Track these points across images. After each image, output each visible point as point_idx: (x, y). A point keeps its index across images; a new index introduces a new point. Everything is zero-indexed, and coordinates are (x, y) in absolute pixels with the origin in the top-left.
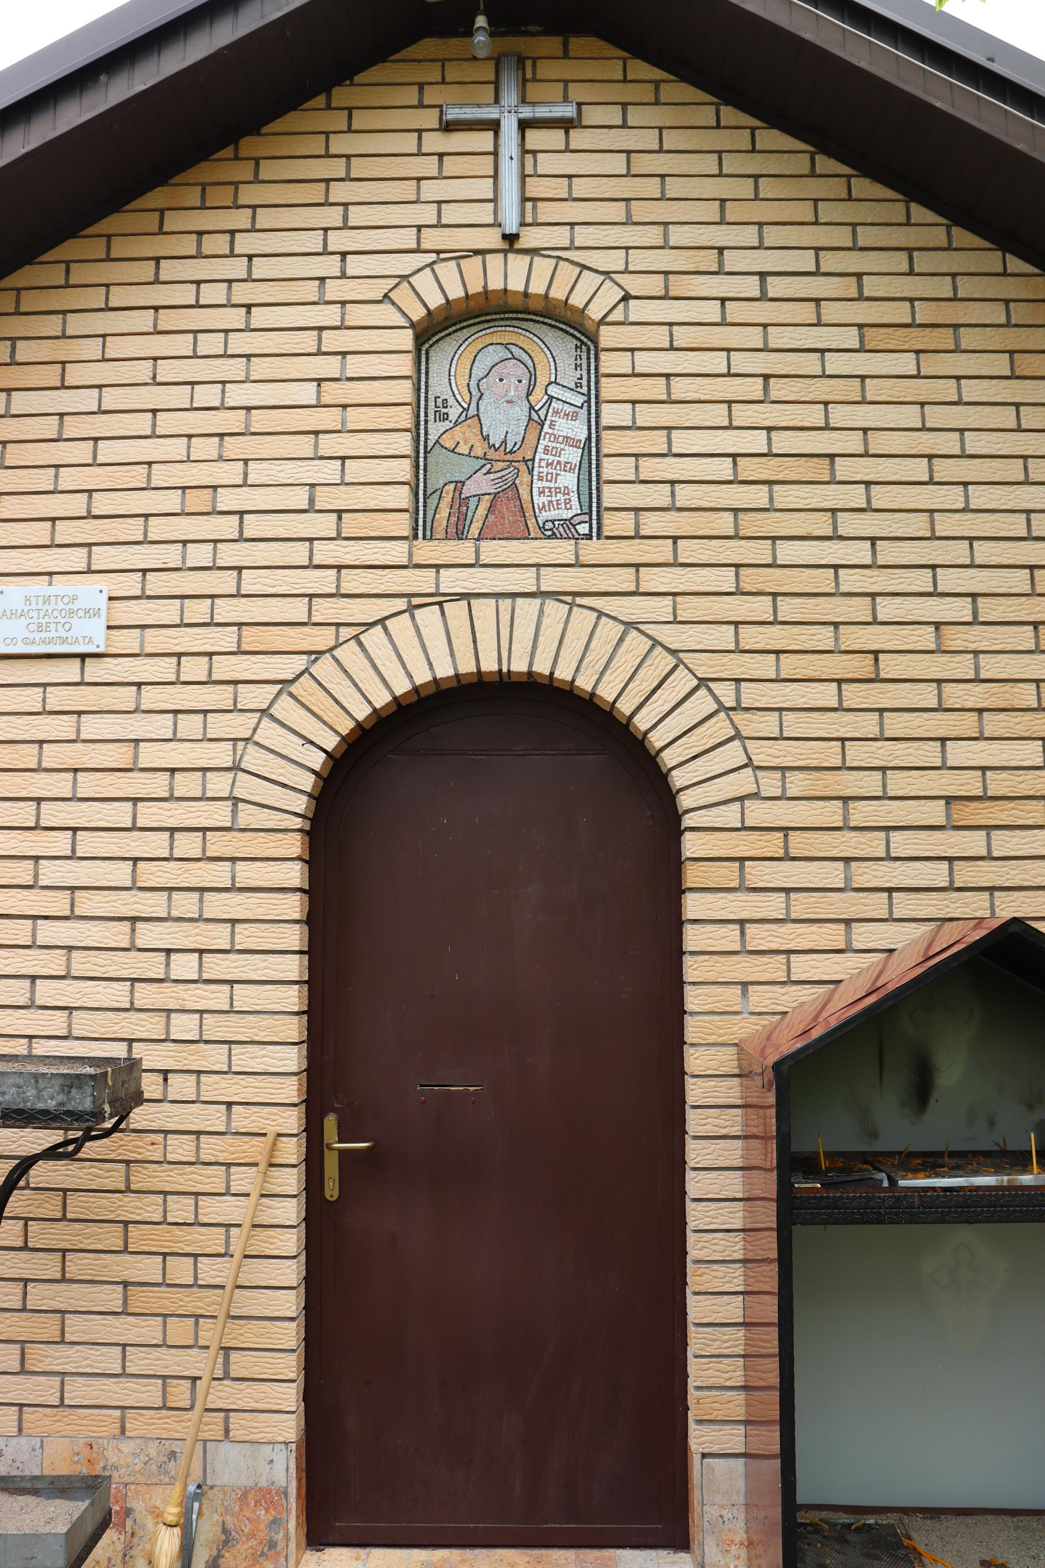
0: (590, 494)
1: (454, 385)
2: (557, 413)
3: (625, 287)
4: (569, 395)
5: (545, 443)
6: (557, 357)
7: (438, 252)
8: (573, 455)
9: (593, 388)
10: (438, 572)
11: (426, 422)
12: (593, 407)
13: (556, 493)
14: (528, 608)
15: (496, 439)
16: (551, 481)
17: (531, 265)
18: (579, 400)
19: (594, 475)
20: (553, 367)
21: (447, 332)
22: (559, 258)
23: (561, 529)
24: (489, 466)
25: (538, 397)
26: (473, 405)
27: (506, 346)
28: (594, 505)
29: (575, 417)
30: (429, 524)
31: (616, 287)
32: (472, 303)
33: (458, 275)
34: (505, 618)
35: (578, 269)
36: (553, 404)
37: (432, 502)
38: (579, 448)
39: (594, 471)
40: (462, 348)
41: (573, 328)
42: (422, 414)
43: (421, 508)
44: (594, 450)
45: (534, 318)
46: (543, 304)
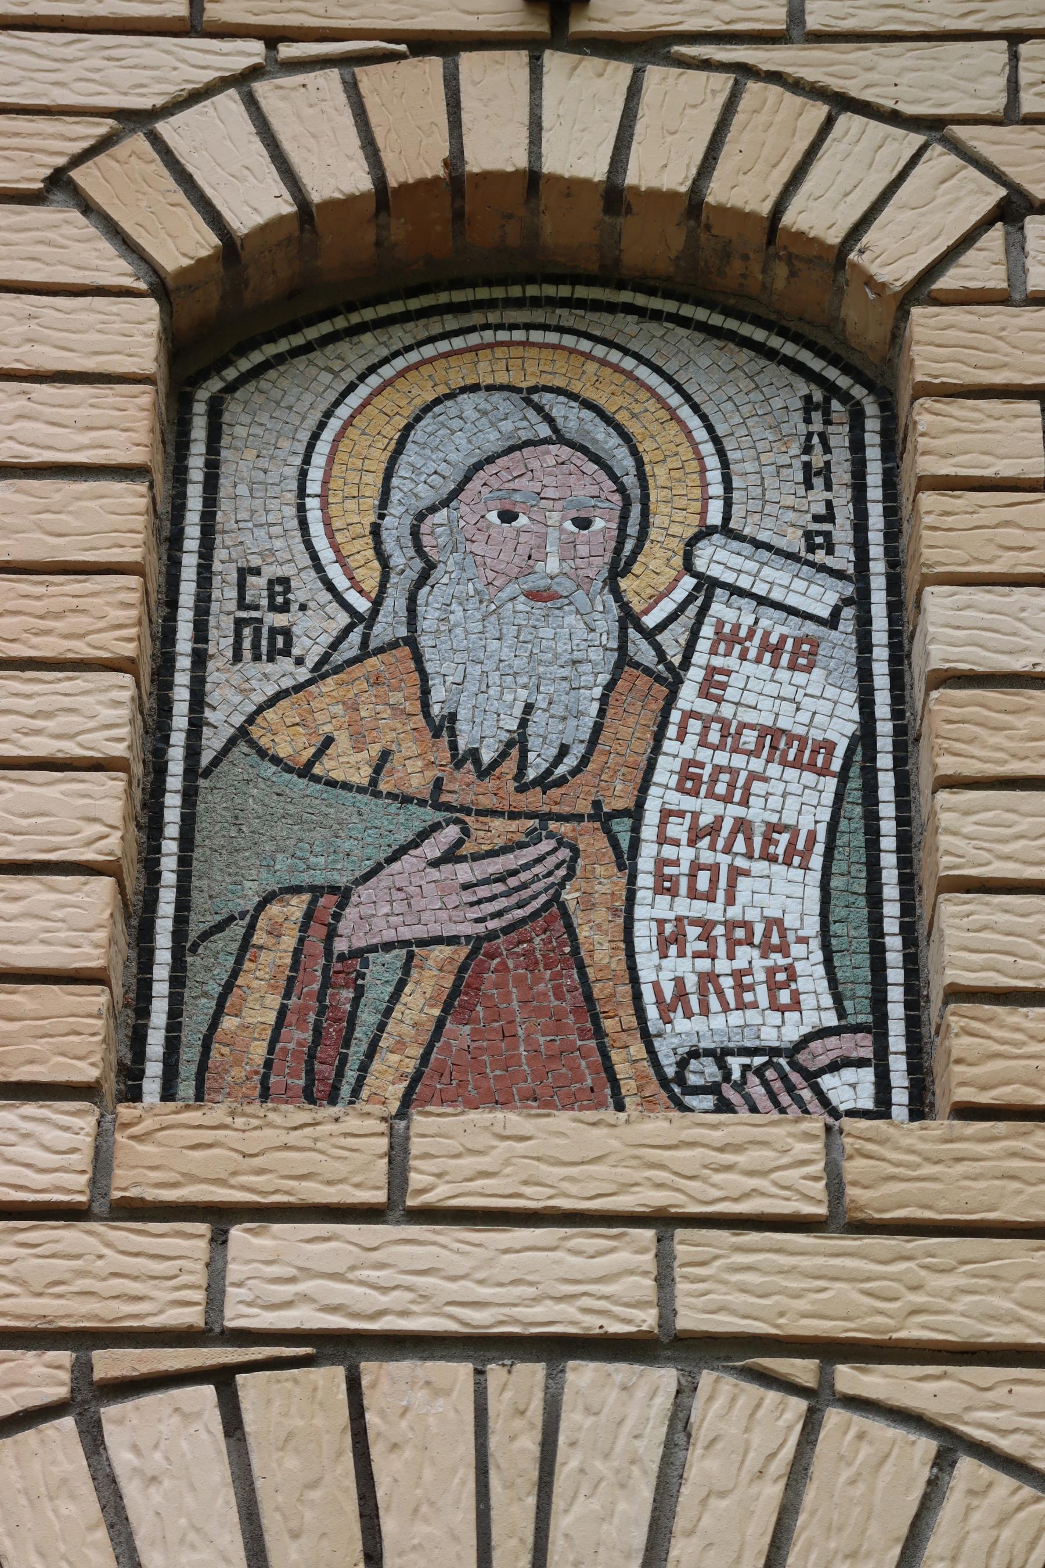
0: (878, 951)
1: (317, 529)
2: (733, 639)
3: (1011, 172)
4: (782, 577)
5: (687, 749)
6: (729, 448)
7: (272, 37)
8: (804, 802)
9: (876, 551)
10: (219, 1240)
11: (200, 659)
12: (880, 623)
13: (733, 944)
14: (618, 1408)
15: (483, 732)
16: (710, 897)
17: (634, 92)
18: (821, 597)
19: (890, 876)
20: (714, 476)
21: (297, 340)
22: (745, 71)
23: (755, 1089)
24: (452, 832)
25: (657, 584)
26: (395, 602)
27: (528, 396)
28: (896, 994)
29: (804, 656)
30: (189, 1054)
31: (972, 172)
32: (398, 229)
33: (347, 120)
34: (516, 1448)
35: (820, 111)
36: (717, 608)
37: (209, 968)
38: (823, 772)
39: (889, 861)
40: (354, 400)
41: (796, 338)
42: (185, 630)
43: (161, 988)
44: (886, 782)
45: (641, 300)
46: (678, 241)
